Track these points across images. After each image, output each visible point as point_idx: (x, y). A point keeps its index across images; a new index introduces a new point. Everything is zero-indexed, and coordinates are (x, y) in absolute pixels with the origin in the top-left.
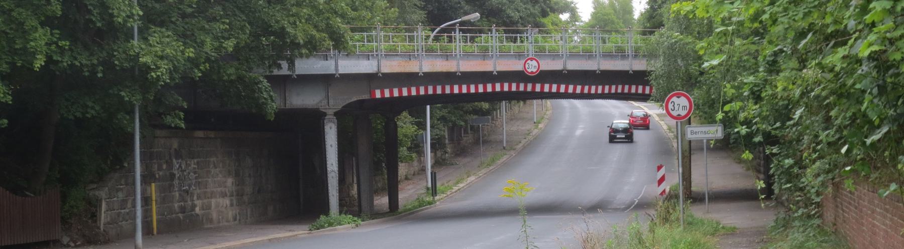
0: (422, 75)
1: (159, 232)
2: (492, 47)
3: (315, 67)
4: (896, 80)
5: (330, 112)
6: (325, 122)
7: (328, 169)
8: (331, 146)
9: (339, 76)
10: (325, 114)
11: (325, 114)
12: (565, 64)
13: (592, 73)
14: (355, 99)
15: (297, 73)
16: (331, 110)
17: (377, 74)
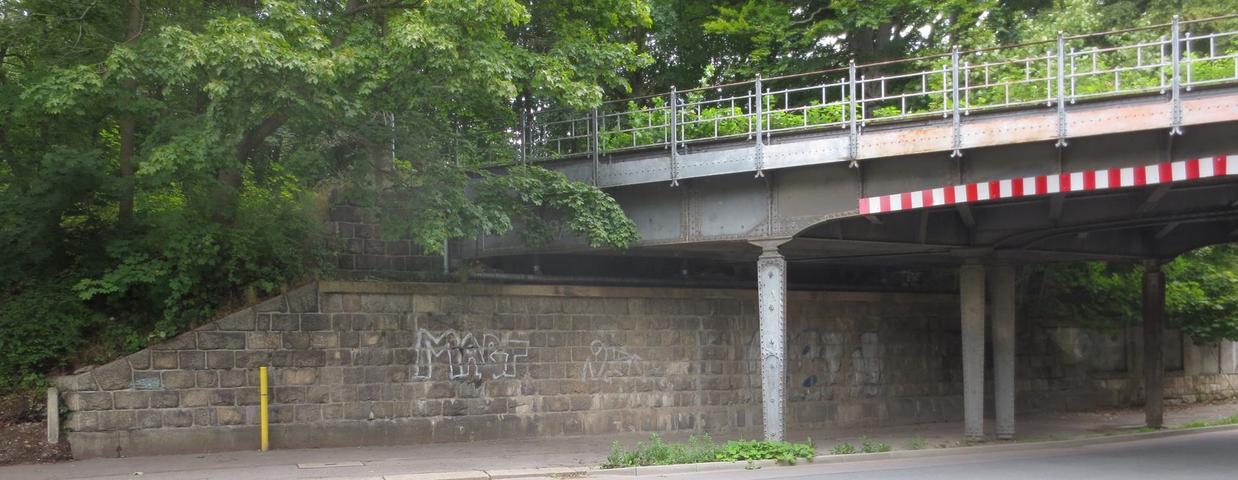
0: (960, 155)
1: (272, 447)
2: (1045, 61)
3: (716, 162)
4: (471, 115)
5: (773, 245)
6: (759, 264)
7: (764, 352)
8: (771, 309)
9: (1180, 133)
10: (759, 251)
11: (759, 251)
12: (853, 146)
13: (941, 158)
14: (826, 218)
15: (680, 177)
16: (770, 243)
17: (847, 163)
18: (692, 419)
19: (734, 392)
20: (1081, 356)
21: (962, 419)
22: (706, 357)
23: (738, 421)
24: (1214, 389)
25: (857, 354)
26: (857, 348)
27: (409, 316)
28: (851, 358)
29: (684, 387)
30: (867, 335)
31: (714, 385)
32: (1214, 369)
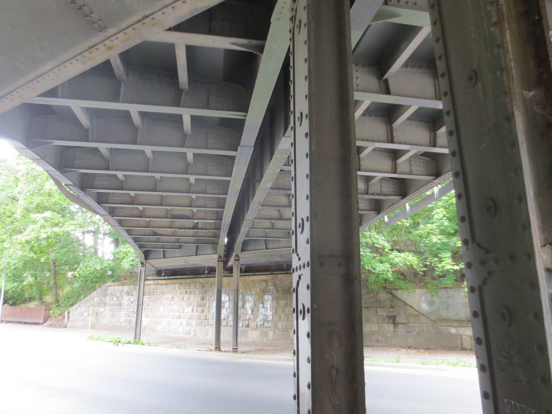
18: (190, 331)
19: (207, 321)
20: (427, 308)
22: (197, 306)
28: (258, 307)
30: (266, 296)
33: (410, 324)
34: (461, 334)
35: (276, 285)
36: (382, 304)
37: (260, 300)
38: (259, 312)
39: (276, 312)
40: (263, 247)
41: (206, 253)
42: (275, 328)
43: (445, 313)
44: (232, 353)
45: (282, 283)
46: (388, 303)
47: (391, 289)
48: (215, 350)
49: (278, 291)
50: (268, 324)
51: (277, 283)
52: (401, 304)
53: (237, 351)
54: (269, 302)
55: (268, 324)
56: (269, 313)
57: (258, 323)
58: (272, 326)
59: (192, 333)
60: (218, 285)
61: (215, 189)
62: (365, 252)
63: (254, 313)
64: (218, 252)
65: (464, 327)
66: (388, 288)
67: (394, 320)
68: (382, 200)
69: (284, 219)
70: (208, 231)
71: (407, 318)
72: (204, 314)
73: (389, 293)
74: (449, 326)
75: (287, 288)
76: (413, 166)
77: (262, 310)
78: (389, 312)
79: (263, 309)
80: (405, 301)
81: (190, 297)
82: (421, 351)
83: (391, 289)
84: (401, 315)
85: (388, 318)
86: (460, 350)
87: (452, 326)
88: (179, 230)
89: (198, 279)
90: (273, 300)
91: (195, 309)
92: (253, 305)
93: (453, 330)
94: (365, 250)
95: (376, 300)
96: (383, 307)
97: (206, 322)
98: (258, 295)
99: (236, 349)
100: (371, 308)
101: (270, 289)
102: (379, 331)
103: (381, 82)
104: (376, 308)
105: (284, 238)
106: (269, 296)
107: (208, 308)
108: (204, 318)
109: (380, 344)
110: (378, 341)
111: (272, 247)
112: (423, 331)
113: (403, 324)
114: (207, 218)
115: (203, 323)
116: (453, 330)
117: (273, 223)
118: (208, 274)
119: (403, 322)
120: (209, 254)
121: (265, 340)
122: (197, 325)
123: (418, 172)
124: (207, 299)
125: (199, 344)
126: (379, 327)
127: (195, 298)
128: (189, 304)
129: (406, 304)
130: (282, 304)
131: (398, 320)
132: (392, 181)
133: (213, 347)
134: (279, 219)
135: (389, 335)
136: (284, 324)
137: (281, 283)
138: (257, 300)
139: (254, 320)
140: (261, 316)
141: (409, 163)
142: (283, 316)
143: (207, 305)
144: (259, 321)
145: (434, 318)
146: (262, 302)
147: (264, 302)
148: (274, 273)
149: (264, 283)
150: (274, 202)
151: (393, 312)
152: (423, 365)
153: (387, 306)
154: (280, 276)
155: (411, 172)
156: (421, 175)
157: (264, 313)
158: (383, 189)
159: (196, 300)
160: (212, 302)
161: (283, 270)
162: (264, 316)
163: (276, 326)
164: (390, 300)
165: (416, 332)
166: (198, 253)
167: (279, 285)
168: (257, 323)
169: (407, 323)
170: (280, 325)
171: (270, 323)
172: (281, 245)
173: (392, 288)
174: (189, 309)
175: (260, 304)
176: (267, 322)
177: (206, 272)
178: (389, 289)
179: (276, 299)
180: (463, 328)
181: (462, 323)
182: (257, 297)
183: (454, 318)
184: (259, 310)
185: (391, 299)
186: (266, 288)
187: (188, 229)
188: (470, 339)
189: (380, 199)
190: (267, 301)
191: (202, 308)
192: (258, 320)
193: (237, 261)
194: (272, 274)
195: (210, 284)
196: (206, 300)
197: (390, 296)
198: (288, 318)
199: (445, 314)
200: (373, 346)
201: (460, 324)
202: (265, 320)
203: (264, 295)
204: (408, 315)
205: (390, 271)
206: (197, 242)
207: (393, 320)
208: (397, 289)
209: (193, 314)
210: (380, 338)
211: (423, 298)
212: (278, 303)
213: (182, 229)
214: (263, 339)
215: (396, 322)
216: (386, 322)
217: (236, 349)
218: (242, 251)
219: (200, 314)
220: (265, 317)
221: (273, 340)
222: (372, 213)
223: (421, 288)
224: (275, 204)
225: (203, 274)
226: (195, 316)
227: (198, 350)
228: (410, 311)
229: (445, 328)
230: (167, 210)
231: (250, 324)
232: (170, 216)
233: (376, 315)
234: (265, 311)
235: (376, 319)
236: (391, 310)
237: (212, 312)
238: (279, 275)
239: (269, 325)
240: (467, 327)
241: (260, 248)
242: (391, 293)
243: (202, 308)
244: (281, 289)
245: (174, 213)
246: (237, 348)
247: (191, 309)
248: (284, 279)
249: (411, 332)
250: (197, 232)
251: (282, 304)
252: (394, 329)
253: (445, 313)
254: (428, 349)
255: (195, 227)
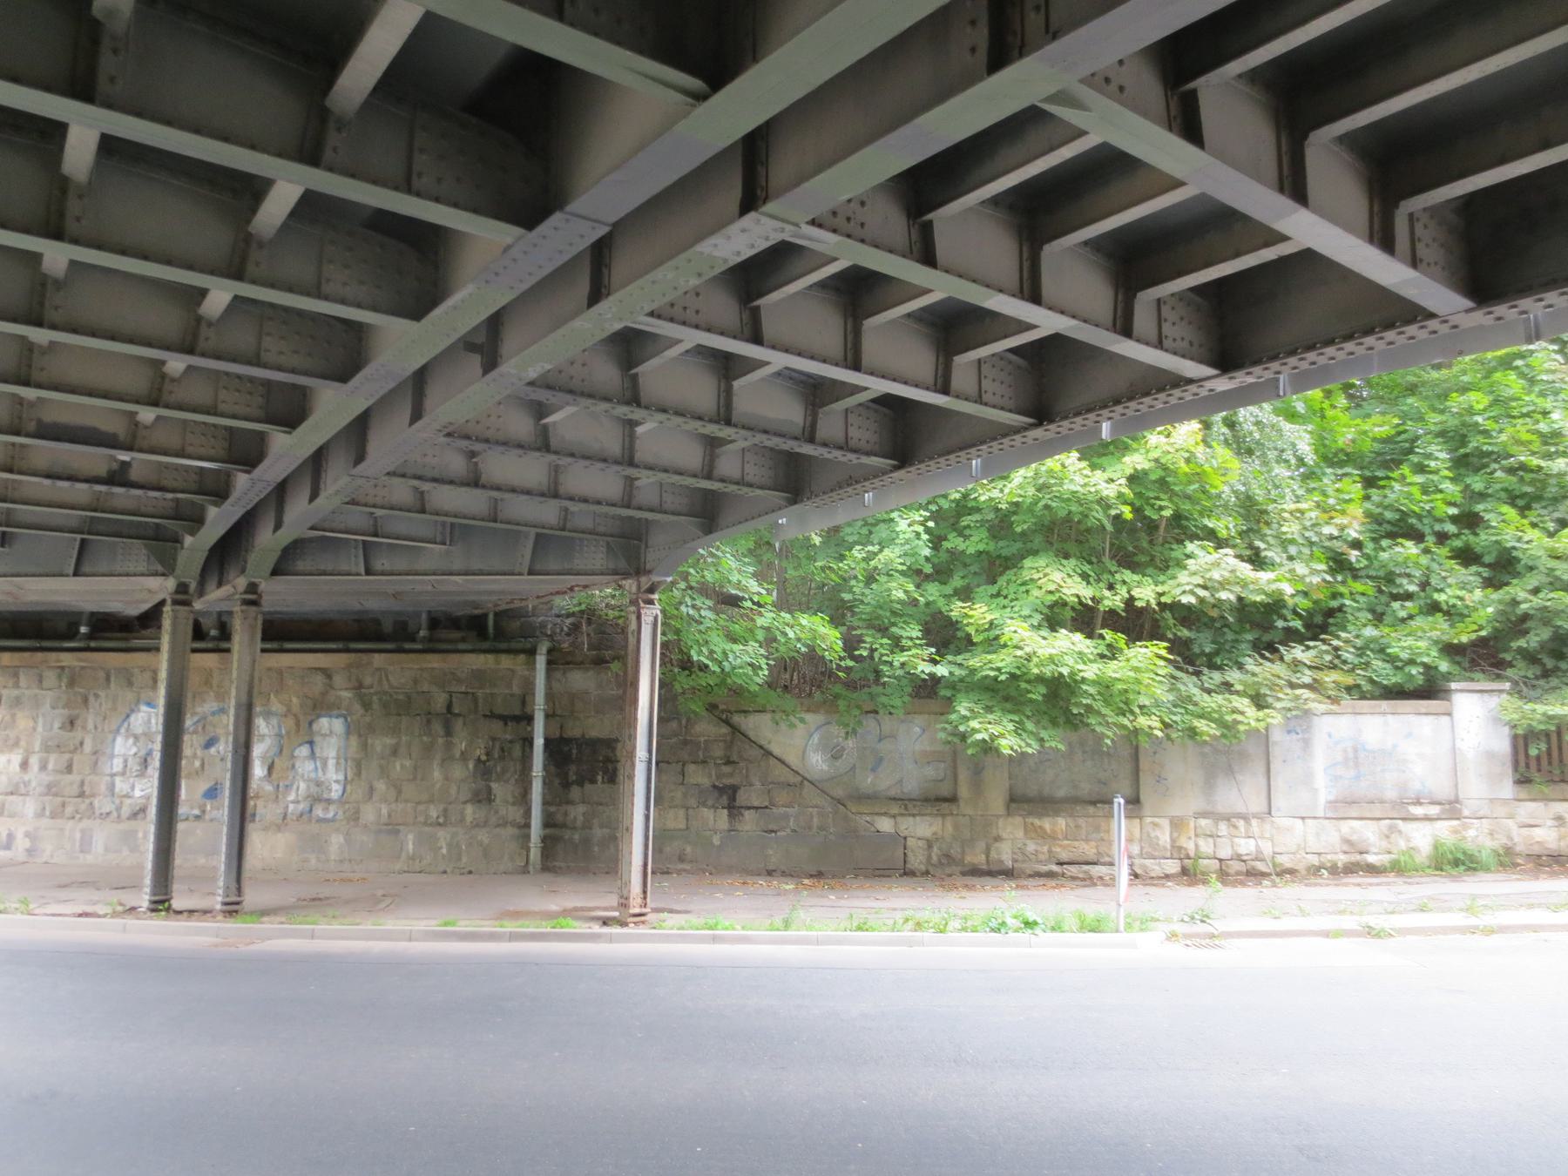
18: (11, 837)
19: (87, 801)
20: (825, 767)
21: (368, 325)
22: (47, 749)
23: (81, 845)
24: (1242, 851)
25: (304, 751)
26: (307, 742)
27: (682, 643)
28: (293, 757)
29: (9, 790)
30: (324, 722)
31: (54, 790)
32: (1256, 804)
33: (775, 810)
34: (906, 833)
35: (360, 686)
36: (700, 753)
37: (302, 731)
38: (297, 773)
39: (358, 774)
40: (357, 564)
41: (118, 568)
42: (352, 823)
43: (869, 780)
44: (220, 917)
45: (385, 682)
46: (718, 751)
47: (729, 712)
48: (153, 910)
49: (367, 706)
50: (326, 810)
51: (368, 681)
52: (756, 752)
53: (236, 912)
54: (333, 740)
55: (326, 810)
56: (334, 778)
57: (291, 807)
58: (340, 815)
59: (21, 843)
60: (170, 687)
61: (295, 352)
62: (699, 610)
63: (274, 776)
64: (178, 571)
65: (914, 815)
66: (722, 707)
67: (733, 798)
68: (808, 458)
69: (484, 487)
70: (170, 496)
71: (769, 791)
72: (75, 778)
73: (723, 721)
74: (877, 814)
75: (401, 697)
76: (985, 377)
77: (306, 767)
78: (719, 777)
79: (312, 762)
80: (766, 746)
81: (13, 716)
82: (806, 881)
83: (729, 712)
84: (751, 785)
85: (716, 794)
86: (901, 876)
87: (885, 814)
88: (47, 482)
89: (53, 656)
90: (348, 733)
91: (34, 761)
92: (275, 750)
93: (885, 825)
94: (698, 603)
95: (685, 742)
96: (704, 762)
97: (83, 807)
98: (295, 715)
99: (237, 903)
100: (668, 763)
101: (339, 697)
102: (687, 828)
103: (1172, 98)
104: (683, 765)
105: (436, 543)
106: (334, 720)
107: (94, 757)
108: (75, 790)
109: (687, 866)
110: (681, 859)
111: (387, 567)
112: (810, 828)
113: (757, 808)
114: (190, 450)
115: (69, 810)
116: (885, 825)
117: (422, 493)
118: (90, 636)
119: (756, 804)
120: (135, 575)
121: (313, 861)
122: (40, 814)
123: (997, 400)
124: (90, 726)
125: (65, 886)
126: (687, 820)
127: (35, 722)
128: (11, 742)
129: (769, 753)
130: (379, 749)
131: (742, 798)
132: (876, 411)
133: (144, 900)
134: (468, 485)
135: (716, 841)
136: (385, 811)
137: (380, 680)
138: (288, 733)
139: (274, 797)
140: (303, 786)
141: (976, 370)
142: (381, 786)
143: (88, 747)
144: (293, 802)
145: (839, 792)
146: (306, 739)
147: (317, 739)
148: (353, 645)
149: (319, 679)
150: (488, 428)
151: (731, 775)
152: (860, 933)
153: (715, 759)
154: (378, 659)
155: (980, 397)
156: (1002, 409)
157: (313, 775)
158: (854, 433)
159: (40, 729)
160: (110, 737)
161: (380, 637)
162: (312, 785)
163: (355, 817)
164: (725, 741)
165: (788, 830)
166: (86, 568)
167: (372, 687)
168: (287, 807)
169: (766, 807)
170: (369, 814)
171: (332, 809)
172: (422, 565)
173: (733, 709)
174: (9, 761)
175: (300, 745)
176: (323, 804)
177: (83, 630)
178: (723, 711)
179: (360, 731)
180: (911, 819)
181: (910, 806)
182: (290, 722)
183: (892, 793)
184: (293, 766)
185: (728, 738)
186: (324, 694)
187: (86, 481)
188: (926, 847)
189: (798, 453)
190: (325, 735)
191: (67, 756)
192: (292, 797)
193: (254, 608)
194: (348, 651)
195: (102, 674)
196: (84, 728)
197: (725, 730)
198: (399, 792)
199: (867, 781)
200: (668, 873)
201: (906, 808)
202: (315, 799)
203: (319, 716)
204: (773, 783)
205: (765, 667)
206: (91, 527)
207: (728, 797)
208: (745, 712)
209: (26, 778)
210: (689, 849)
211: (816, 738)
212: (364, 746)
213: (60, 478)
214: (306, 860)
215: (737, 804)
216: (710, 803)
217: (237, 903)
218: (276, 572)
219: (59, 777)
220: (316, 789)
221: (341, 861)
222: (776, 497)
223: (813, 712)
224: (489, 434)
225: (71, 634)
226: (34, 784)
227: (80, 915)
228: (779, 772)
229: (868, 818)
230: (20, 401)
231: (257, 812)
232: (32, 426)
233: (682, 784)
234: (316, 768)
235: (679, 794)
236: (727, 769)
237: (108, 771)
238: (376, 655)
239: (330, 815)
240: (923, 815)
241: (344, 567)
242: (727, 722)
243: (67, 756)
244: (380, 700)
245: (50, 416)
246: (239, 899)
247: (16, 758)
248: (391, 668)
249: (775, 832)
250: (106, 493)
251: (379, 749)
252: (730, 822)
253: (869, 780)
254: (819, 875)
255: (118, 477)
